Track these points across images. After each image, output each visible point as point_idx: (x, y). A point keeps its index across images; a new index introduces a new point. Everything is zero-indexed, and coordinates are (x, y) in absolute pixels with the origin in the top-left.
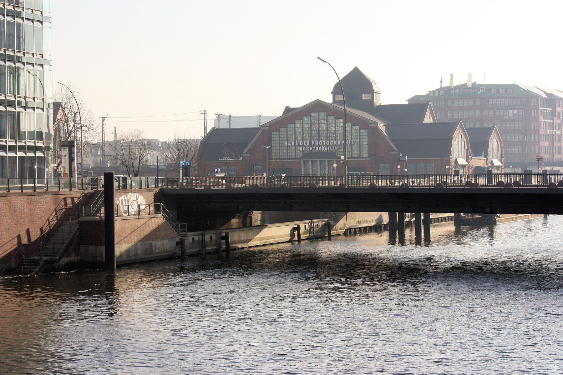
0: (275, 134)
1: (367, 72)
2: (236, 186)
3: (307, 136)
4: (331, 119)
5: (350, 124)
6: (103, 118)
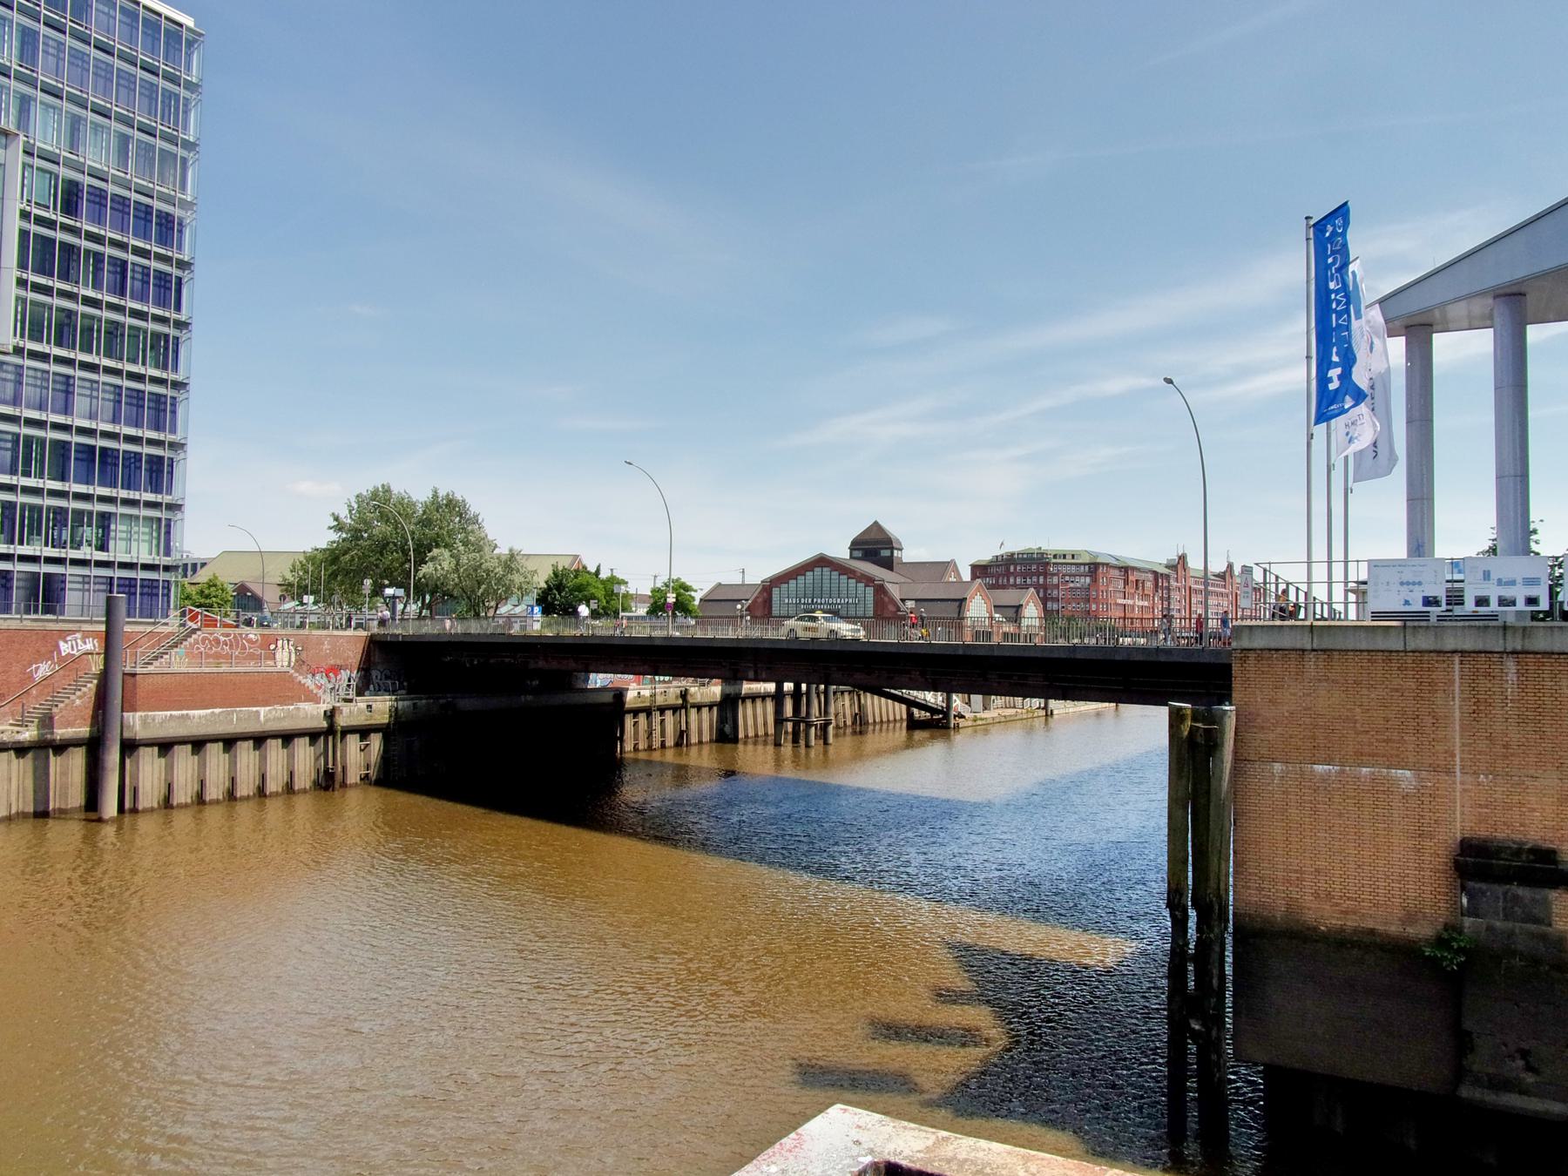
0: (775, 591)
1: (893, 528)
2: (1410, 930)
3: (809, 592)
4: (835, 574)
5: (863, 585)
6: (655, 577)
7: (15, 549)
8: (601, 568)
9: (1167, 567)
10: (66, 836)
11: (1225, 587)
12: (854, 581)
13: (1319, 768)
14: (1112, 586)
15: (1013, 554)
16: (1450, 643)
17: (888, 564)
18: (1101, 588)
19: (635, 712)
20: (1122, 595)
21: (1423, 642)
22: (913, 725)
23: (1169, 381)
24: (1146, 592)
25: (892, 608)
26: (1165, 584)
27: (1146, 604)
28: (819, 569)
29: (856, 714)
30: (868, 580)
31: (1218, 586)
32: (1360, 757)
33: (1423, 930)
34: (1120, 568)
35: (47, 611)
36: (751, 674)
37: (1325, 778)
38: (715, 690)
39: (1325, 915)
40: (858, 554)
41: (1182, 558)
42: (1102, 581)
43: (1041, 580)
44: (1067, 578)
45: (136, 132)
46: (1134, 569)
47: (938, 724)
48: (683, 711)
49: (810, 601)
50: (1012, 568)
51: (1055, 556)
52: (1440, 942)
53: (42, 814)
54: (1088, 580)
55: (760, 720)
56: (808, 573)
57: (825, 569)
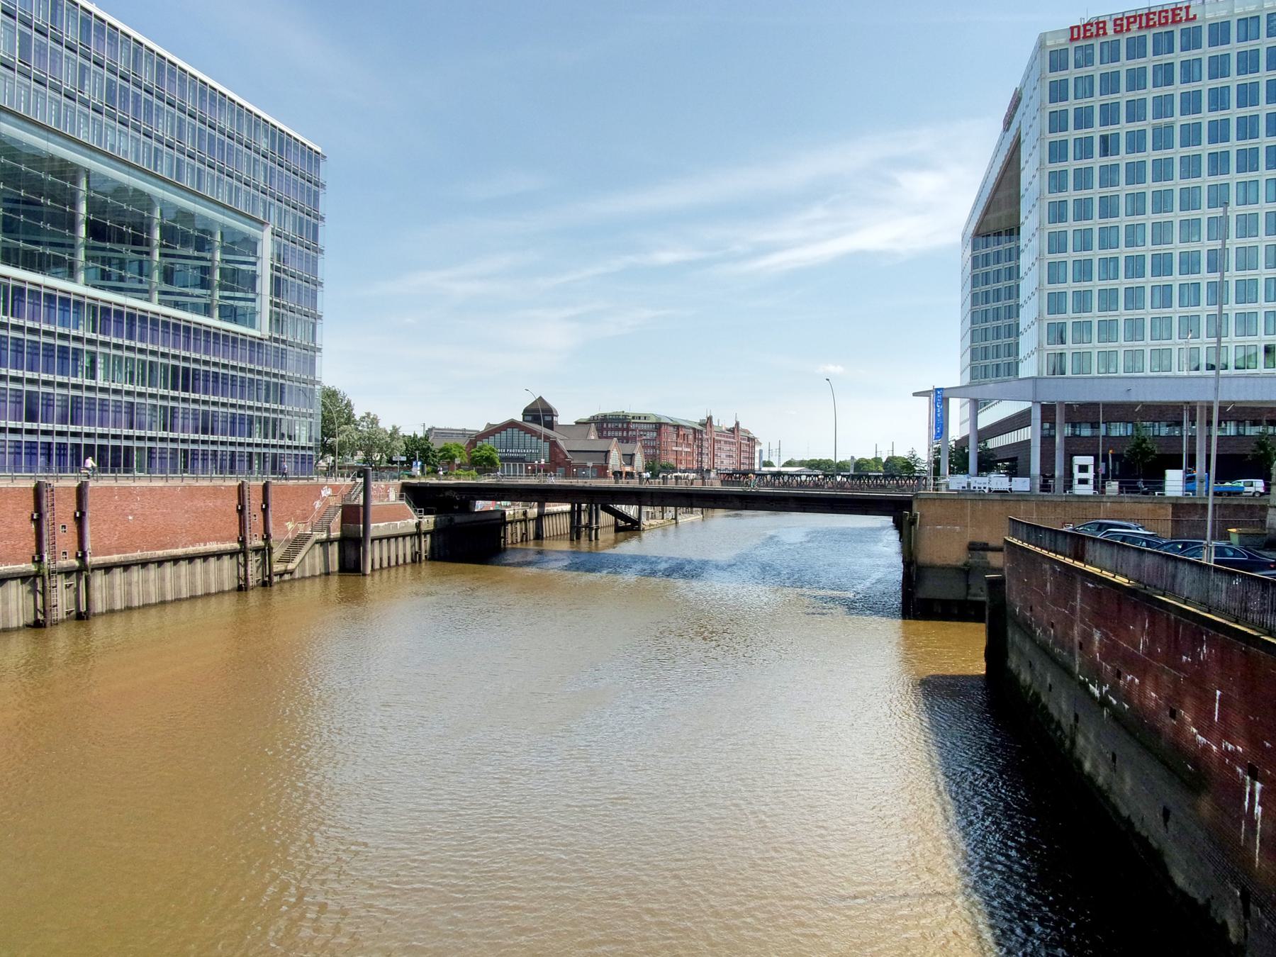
1: (552, 402)
4: (522, 433)
9: (700, 425)
11: (734, 438)
12: (535, 438)
13: (939, 527)
14: (669, 436)
15: (605, 416)
16: (968, 497)
17: (550, 425)
19: (511, 522)
21: (963, 497)
22: (618, 529)
23: (828, 380)
27: (689, 450)
30: (547, 438)
31: (730, 437)
32: (948, 524)
33: (960, 563)
34: (674, 426)
35: (126, 472)
36: (649, 503)
37: (939, 529)
38: (533, 511)
39: (938, 562)
40: (530, 418)
41: (710, 419)
42: (664, 435)
43: (625, 434)
44: (642, 433)
45: (186, 157)
46: (684, 427)
50: (605, 425)
51: (633, 418)
52: (965, 565)
54: (655, 434)
57: (515, 430)
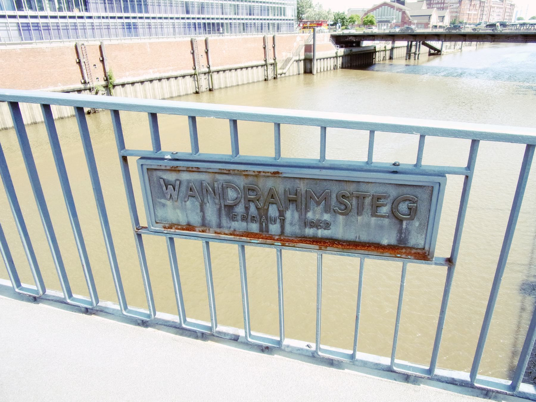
3: (380, 14)
7: (38, 13)
8: (529, 18)
10: (271, 83)
18: (462, 8)
19: (379, 51)
20: (469, 10)
24: (476, 8)
25: (407, 19)
26: (483, 5)
28: (384, 6)
29: (384, 57)
30: (400, 10)
31: (500, 5)
44: (451, 5)
47: (437, 53)
48: (265, 66)
49: (380, 17)
53: (299, 74)
54: (458, 5)
55: (403, 53)
56: (377, 10)
57: (386, 6)
